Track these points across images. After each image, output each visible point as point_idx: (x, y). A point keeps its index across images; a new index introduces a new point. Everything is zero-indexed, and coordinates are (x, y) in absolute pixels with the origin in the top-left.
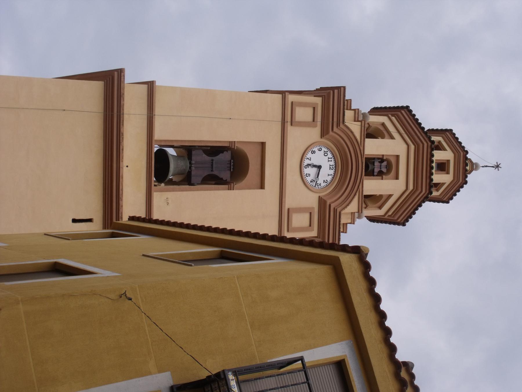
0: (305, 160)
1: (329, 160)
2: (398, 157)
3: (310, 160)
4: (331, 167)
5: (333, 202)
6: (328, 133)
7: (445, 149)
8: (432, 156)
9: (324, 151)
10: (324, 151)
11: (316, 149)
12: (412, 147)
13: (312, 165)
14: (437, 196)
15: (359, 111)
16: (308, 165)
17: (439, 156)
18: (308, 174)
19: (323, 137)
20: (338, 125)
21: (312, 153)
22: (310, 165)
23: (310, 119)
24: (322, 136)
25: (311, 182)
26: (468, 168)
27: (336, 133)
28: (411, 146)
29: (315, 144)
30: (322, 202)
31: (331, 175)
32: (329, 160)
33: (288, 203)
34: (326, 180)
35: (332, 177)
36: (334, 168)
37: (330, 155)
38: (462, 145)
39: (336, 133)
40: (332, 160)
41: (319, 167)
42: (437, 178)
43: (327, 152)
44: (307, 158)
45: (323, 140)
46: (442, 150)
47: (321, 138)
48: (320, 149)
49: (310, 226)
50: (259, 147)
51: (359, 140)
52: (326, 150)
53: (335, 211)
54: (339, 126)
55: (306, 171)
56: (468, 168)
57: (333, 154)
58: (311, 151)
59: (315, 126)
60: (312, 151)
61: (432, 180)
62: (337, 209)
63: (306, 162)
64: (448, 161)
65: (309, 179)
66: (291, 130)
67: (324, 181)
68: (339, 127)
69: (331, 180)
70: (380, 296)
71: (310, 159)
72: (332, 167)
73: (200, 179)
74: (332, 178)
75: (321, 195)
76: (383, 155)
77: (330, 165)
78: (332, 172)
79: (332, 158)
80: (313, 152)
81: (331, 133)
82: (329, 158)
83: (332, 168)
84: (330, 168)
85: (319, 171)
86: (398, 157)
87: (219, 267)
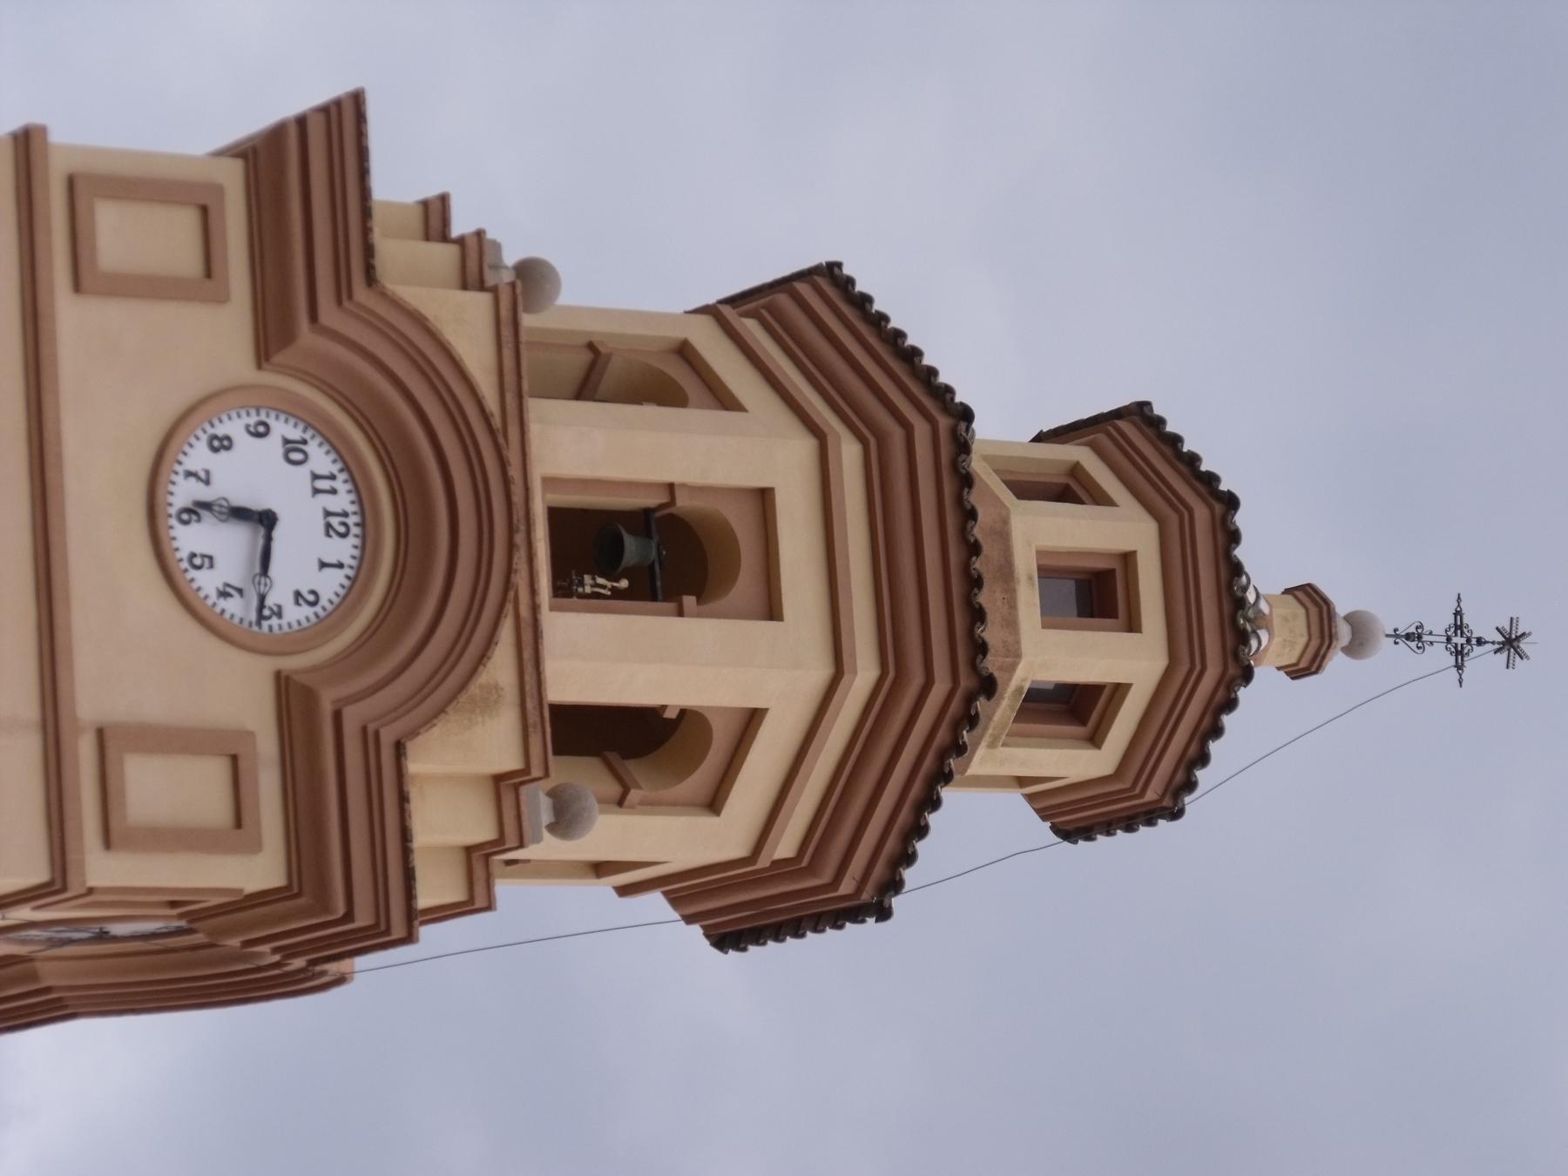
0: (179, 479)
2: (764, 498)
3: (207, 482)
4: (335, 521)
6: (287, 337)
7: (1100, 498)
9: (286, 441)
10: (286, 441)
12: (849, 454)
13: (221, 506)
15: (487, 250)
16: (196, 510)
18: (203, 556)
19: (267, 359)
20: (342, 292)
21: (215, 450)
22: (207, 506)
23: (183, 256)
25: (224, 594)
28: (839, 437)
31: (340, 566)
34: (313, 592)
35: (348, 577)
36: (355, 530)
37: (321, 459)
38: (1203, 468)
40: (341, 484)
41: (266, 520)
43: (305, 442)
44: (189, 474)
45: (269, 378)
46: (1080, 502)
47: (259, 367)
48: (261, 429)
49: (238, 824)
52: (295, 434)
53: (369, 739)
54: (350, 296)
55: (188, 539)
58: (204, 438)
59: (221, 298)
60: (215, 437)
62: (377, 734)
63: (183, 493)
64: (1128, 558)
67: (298, 594)
68: (346, 304)
71: (202, 475)
72: (344, 524)
74: (347, 583)
75: (290, 663)
76: (671, 487)
77: (328, 514)
78: (344, 549)
79: (332, 477)
80: (221, 444)
81: (306, 335)
82: (315, 477)
83: (342, 529)
84: (328, 526)
85: (269, 539)
86: (764, 498)
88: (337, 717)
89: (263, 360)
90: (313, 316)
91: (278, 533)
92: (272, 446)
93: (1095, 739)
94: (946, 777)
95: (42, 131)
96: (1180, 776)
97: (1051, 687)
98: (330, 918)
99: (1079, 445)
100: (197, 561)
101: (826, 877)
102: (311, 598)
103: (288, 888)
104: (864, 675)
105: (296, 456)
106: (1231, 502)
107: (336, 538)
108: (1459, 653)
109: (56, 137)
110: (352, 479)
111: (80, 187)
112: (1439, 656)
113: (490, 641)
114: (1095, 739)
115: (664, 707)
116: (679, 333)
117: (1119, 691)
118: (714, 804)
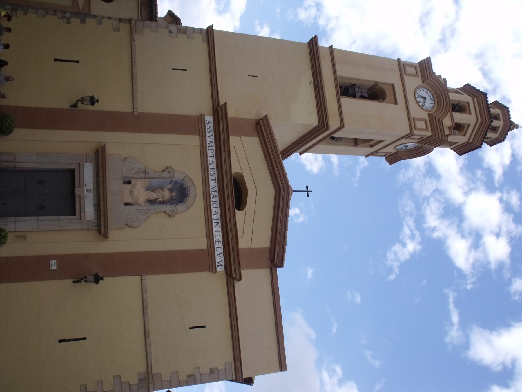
1: (429, 96)
4: (431, 99)
5: (437, 115)
6: (426, 80)
12: (475, 99)
17: (495, 123)
23: (415, 73)
24: (423, 82)
26: (512, 127)
30: (430, 115)
32: (429, 96)
33: (413, 115)
37: (429, 93)
41: (425, 98)
44: (417, 93)
47: (423, 83)
50: (391, 87)
52: (427, 91)
53: (439, 119)
56: (512, 127)
57: (431, 93)
62: (439, 119)
63: (417, 95)
65: (421, 104)
66: (405, 78)
73: (359, 96)
75: (430, 112)
76: (460, 101)
78: (433, 102)
81: (427, 80)
82: (429, 95)
84: (431, 100)
85: (425, 100)
86: (468, 103)
88: (435, 117)
91: (426, 100)
92: (425, 91)
93: (496, 133)
95: (400, 59)
98: (436, 138)
99: (456, 143)
103: (432, 135)
104: (480, 120)
110: (432, 95)
113: (447, 114)
114: (496, 133)
115: (461, 123)
117: (499, 127)
118: (465, 135)
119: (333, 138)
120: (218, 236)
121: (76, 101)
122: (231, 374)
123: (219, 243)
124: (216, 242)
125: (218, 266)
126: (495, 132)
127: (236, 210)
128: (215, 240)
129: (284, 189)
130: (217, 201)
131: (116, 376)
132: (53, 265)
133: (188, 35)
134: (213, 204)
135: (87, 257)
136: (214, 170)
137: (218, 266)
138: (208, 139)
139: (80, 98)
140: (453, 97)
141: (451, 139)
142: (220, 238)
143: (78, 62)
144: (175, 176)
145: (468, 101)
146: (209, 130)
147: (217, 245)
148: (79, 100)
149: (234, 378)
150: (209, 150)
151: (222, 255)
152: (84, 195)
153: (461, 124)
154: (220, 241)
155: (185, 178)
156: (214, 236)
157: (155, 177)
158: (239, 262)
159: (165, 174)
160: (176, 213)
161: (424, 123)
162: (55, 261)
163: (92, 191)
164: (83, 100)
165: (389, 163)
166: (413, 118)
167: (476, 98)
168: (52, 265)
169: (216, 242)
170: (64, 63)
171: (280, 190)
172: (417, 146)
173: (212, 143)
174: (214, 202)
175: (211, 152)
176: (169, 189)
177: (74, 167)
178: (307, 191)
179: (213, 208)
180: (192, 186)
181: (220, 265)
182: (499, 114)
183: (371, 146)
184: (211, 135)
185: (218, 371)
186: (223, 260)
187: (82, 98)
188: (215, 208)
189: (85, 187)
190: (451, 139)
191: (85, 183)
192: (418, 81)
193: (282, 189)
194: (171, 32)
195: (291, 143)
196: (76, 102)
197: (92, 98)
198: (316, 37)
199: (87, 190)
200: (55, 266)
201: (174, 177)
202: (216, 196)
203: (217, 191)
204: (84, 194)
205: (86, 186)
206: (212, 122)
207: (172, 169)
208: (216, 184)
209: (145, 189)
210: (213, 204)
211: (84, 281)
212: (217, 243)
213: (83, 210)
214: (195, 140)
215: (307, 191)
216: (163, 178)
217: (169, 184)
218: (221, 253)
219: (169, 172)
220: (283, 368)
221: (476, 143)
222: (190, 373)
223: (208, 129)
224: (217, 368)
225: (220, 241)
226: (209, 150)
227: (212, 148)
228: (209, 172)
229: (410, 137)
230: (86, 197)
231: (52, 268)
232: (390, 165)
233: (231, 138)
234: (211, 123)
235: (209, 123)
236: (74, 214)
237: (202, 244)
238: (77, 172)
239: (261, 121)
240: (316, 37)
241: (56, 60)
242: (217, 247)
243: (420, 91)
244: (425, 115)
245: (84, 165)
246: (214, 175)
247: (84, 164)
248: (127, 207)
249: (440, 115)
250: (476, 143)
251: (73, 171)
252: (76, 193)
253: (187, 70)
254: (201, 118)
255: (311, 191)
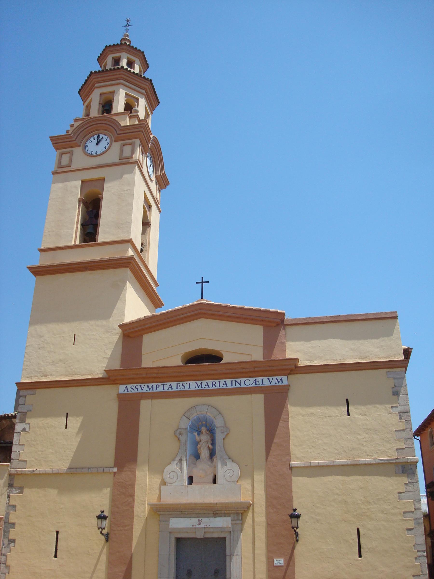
0: (92, 154)
1: (94, 139)
5: (117, 132)
8: (110, 69)
9: (89, 143)
10: (89, 143)
11: (87, 149)
12: (96, 85)
14: (139, 60)
20: (71, 138)
23: (68, 155)
24: (79, 146)
26: (128, 44)
27: (76, 138)
29: (111, 142)
32: (94, 139)
33: (116, 159)
34: (106, 139)
39: (76, 138)
42: (136, 69)
44: (92, 153)
48: (87, 146)
51: (82, 122)
56: (128, 44)
58: (88, 152)
61: (137, 74)
67: (106, 140)
69: (91, 138)
70: (202, 348)
76: (99, 104)
82: (93, 140)
86: (101, 94)
87: (146, 207)
89: (131, 161)
90: (75, 140)
94: (426, 550)
96: (138, 51)
97: (429, 540)
100: (101, 151)
101: (147, 87)
102: (106, 139)
104: (122, 81)
105: (91, 142)
106: (106, 46)
107: (100, 137)
108: (129, 26)
109: (53, 170)
110: (93, 136)
111: (58, 167)
112: (129, 28)
115: (124, 103)
116: (85, 107)
119: (142, 250)
120: (250, 382)
121: (102, 535)
122: (399, 372)
123: (257, 381)
124: (256, 384)
125: (282, 383)
126: (133, 62)
127: (222, 362)
128: (254, 385)
129: (200, 309)
130: (212, 382)
131: (399, 497)
132: (280, 562)
133: (28, 411)
134: (216, 387)
135: (270, 525)
136: (178, 385)
137: (282, 383)
138: (145, 390)
139: (99, 531)
140: (95, 112)
141: (142, 116)
142: (253, 379)
143: (57, 532)
144: (185, 428)
145: (99, 94)
146: (134, 388)
147: (259, 383)
148: (101, 532)
149: (404, 369)
150: (156, 390)
151: (271, 378)
152: (205, 528)
153: (126, 102)
154: (256, 380)
155: (187, 417)
156: (250, 386)
157: (186, 449)
158: (150, 189)
159: (183, 438)
160: (225, 426)
161: (125, 147)
162: (275, 560)
163: (200, 519)
164: (101, 528)
165: (167, 185)
166: (120, 159)
167: (95, 85)
168: (279, 563)
169: (256, 384)
170: (58, 548)
171: (201, 313)
172: (151, 155)
173: (149, 386)
174: (214, 386)
175: (159, 387)
176: (199, 435)
177: (174, 538)
178: (202, 282)
179: (219, 386)
180: (196, 409)
181: (281, 381)
182: (113, 58)
183: (150, 207)
184: (140, 387)
185: (395, 386)
186: (276, 377)
187: (99, 528)
188: (220, 384)
189: (196, 527)
190: (142, 116)
191: (191, 527)
192: (78, 152)
193: (200, 311)
194: (24, 430)
195: (146, 296)
196: (103, 535)
197: (99, 517)
198: (30, 268)
199: (199, 524)
200: (280, 560)
201: (186, 429)
202: (207, 383)
203: (201, 381)
204: (203, 528)
205: (194, 526)
206: (126, 385)
207: (177, 430)
208: (194, 382)
209: (197, 461)
210: (216, 387)
211: (297, 530)
212: (257, 383)
213: (222, 529)
214: (145, 404)
215: (202, 282)
216: (186, 441)
217: (193, 434)
218: (269, 379)
219: (180, 434)
220: (394, 315)
221: (146, 85)
222: (397, 417)
223: (134, 390)
224: (392, 388)
225: (256, 380)
226: (156, 390)
227: (155, 387)
228: (181, 389)
229: (141, 164)
230: (206, 526)
231: (282, 564)
232: (169, 184)
233: (143, 366)
234: (126, 387)
235: (127, 389)
236: (225, 539)
237: (260, 398)
238: (179, 536)
239: (125, 332)
240: (30, 268)
241: (56, 556)
242: (262, 384)
243: (89, 150)
244: (116, 146)
245: (172, 527)
246: (184, 384)
247: (170, 527)
248: (218, 480)
249: (116, 128)
250: (146, 85)
251: (178, 540)
252: (202, 537)
253: (67, 412)
254: (122, 398)
255: (202, 278)
